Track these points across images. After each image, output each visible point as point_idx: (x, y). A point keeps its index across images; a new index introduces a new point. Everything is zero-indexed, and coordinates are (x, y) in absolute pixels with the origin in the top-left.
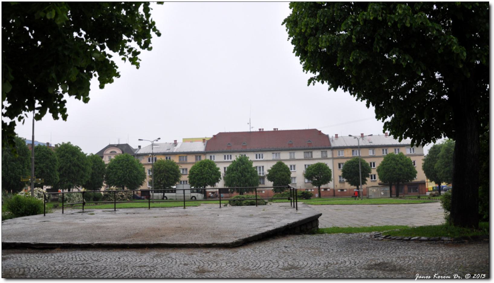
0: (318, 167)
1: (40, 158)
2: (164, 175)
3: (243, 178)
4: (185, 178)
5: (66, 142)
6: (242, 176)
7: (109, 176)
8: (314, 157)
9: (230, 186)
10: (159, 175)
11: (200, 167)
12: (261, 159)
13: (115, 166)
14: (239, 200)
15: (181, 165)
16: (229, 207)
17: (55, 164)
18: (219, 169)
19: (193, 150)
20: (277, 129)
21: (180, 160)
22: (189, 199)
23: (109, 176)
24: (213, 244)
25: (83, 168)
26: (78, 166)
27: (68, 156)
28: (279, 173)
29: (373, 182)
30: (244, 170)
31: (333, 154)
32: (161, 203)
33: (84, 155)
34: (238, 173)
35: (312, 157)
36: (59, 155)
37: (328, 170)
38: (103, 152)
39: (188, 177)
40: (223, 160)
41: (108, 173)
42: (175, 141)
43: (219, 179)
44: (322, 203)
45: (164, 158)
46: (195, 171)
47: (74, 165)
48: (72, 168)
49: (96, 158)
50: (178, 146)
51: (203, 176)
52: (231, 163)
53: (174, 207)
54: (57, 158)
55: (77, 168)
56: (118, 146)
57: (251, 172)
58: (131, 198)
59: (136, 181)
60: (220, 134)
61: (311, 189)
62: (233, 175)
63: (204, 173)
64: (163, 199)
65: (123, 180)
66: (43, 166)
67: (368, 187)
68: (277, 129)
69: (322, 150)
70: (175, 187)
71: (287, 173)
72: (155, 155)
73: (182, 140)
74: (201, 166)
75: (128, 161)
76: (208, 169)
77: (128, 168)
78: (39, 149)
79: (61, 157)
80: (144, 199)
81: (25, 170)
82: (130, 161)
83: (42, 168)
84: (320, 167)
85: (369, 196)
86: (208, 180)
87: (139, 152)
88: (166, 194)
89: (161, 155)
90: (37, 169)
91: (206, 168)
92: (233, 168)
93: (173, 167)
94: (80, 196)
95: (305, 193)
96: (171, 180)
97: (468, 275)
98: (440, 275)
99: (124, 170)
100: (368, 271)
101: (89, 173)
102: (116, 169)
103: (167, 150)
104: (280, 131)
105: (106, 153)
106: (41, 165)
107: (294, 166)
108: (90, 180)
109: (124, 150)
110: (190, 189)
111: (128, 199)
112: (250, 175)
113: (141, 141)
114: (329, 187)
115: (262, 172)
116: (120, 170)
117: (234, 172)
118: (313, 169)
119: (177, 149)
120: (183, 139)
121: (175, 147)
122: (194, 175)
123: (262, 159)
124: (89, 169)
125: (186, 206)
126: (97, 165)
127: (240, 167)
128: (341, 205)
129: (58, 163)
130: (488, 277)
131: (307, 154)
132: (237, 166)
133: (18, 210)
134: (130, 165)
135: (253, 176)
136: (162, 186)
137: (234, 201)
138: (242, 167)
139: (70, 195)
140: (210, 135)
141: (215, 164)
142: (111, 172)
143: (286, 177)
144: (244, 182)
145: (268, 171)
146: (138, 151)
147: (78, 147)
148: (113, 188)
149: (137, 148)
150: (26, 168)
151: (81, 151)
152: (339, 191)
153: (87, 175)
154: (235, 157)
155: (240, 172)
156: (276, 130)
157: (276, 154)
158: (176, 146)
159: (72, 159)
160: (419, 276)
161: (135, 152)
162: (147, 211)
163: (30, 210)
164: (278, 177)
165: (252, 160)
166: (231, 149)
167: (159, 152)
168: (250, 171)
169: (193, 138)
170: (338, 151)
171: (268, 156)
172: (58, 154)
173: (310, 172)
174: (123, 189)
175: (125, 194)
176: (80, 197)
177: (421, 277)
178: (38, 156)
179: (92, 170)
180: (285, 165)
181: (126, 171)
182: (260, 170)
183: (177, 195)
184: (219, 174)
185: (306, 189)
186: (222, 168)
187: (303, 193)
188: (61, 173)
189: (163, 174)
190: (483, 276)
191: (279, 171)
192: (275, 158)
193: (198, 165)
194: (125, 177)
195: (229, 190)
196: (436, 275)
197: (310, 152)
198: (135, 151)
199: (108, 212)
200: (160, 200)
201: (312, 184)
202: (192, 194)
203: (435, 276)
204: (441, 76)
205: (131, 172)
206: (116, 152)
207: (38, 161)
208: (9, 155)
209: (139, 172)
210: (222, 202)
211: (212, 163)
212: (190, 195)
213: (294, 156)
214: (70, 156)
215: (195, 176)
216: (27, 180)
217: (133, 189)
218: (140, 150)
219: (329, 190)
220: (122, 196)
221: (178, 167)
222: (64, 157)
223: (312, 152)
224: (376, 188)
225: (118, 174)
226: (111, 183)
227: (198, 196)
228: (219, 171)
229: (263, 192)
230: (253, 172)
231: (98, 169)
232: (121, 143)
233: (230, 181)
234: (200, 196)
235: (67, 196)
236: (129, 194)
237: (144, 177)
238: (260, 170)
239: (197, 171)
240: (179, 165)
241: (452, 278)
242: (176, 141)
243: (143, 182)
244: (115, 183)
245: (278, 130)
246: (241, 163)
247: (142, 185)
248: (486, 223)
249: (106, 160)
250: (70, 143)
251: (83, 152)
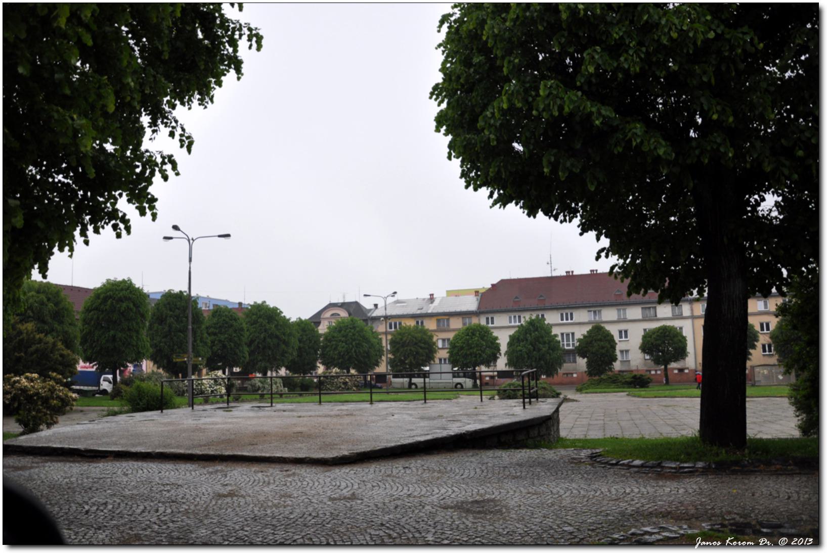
0: (661, 333)
1: (220, 327)
2: (410, 350)
3: (535, 352)
4: (444, 354)
5: (259, 302)
6: (534, 350)
7: (325, 352)
8: (659, 316)
9: (515, 366)
10: (402, 349)
11: (466, 336)
12: (570, 321)
13: (333, 337)
14: (512, 390)
15: (437, 334)
16: (497, 400)
17: (241, 335)
18: (496, 338)
19: (458, 309)
20: (597, 271)
21: (438, 325)
22: (452, 388)
23: (325, 352)
24: (306, 458)
25: (285, 340)
26: (277, 337)
27: (262, 322)
28: (595, 344)
29: (766, 358)
30: (537, 339)
31: (692, 310)
32: (399, 394)
33: (286, 321)
34: (526, 345)
35: (656, 316)
36: (249, 322)
37: (680, 338)
38: (321, 314)
39: (447, 353)
40: (507, 324)
41: (324, 348)
42: (432, 295)
43: (498, 356)
44: (656, 395)
45: (411, 323)
46: (457, 342)
47: (272, 336)
48: (269, 340)
49: (305, 325)
50: (436, 303)
51: (471, 350)
52: (517, 329)
53: (414, 400)
54: (245, 326)
55: (275, 341)
56: (343, 305)
57: (550, 342)
58: (358, 386)
59: (367, 360)
60: (503, 282)
61: (656, 371)
62: (519, 348)
63: (473, 346)
64: (410, 387)
65: (347, 357)
66: (225, 339)
67: (754, 367)
68: (597, 271)
69: (643, 306)
70: (427, 368)
71: (609, 343)
72: (389, 319)
73: (445, 292)
74: (468, 335)
75: (354, 328)
76: (478, 340)
77: (354, 340)
78: (218, 313)
79: (252, 325)
80: (381, 388)
81: (197, 344)
82: (358, 329)
83: (224, 342)
84: (665, 333)
85: (755, 381)
86: (479, 357)
87: (374, 315)
88: (414, 380)
89: (408, 317)
90: (216, 342)
91: (476, 338)
92: (519, 336)
93: (425, 337)
94: (280, 383)
95: (638, 376)
96: (421, 358)
98: (737, 540)
99: (348, 342)
100: (285, 502)
101: (293, 348)
102: (337, 341)
103: (419, 309)
104: (600, 274)
105: (324, 317)
106: (222, 337)
107: (626, 332)
108: (296, 359)
109: (351, 312)
110: (451, 371)
111: (354, 388)
112: (547, 348)
113: (368, 297)
114: (687, 366)
115: (571, 343)
116: (343, 342)
117: (521, 343)
118: (654, 336)
119: (433, 309)
120: (447, 291)
121: (431, 305)
122: (457, 349)
123: (572, 321)
124: (295, 342)
125: (428, 399)
126: (306, 335)
127: (531, 334)
128: (689, 397)
129: (246, 334)
130: (817, 543)
131: (647, 311)
132: (526, 333)
133: (138, 404)
134: (357, 334)
135: (552, 350)
136: (408, 366)
137: (505, 391)
138: (533, 334)
139: (265, 381)
140: (486, 283)
141: (490, 331)
142: (329, 346)
143: (607, 351)
144: (538, 360)
145: (579, 340)
146: (373, 313)
147: (277, 308)
148: (335, 370)
149: (372, 307)
150: (198, 342)
151: (283, 315)
152: (676, 371)
153: (290, 351)
154: (526, 317)
155: (531, 344)
156: (595, 272)
157: (595, 312)
158: (432, 303)
159: (268, 326)
160: (702, 541)
161: (369, 315)
162: (367, 405)
163: (154, 403)
164: (594, 350)
165: (551, 322)
166: (519, 306)
167: (405, 313)
168: (547, 342)
169: (458, 290)
170: (701, 305)
171: (582, 316)
172: (247, 320)
173: (649, 341)
174: (348, 372)
175: (350, 381)
176: (278, 385)
178: (217, 324)
179: (298, 343)
180: (606, 330)
181: (352, 344)
182: (568, 340)
183: (431, 381)
184: (497, 348)
185: (647, 371)
186: (503, 340)
187: (635, 377)
188: (252, 348)
189: (409, 348)
190: (808, 542)
191: (596, 341)
192: (593, 319)
193: (463, 333)
194: (350, 354)
195: (514, 373)
196: (729, 539)
197: (653, 307)
198: (368, 313)
199: (256, 409)
200: (404, 389)
201: (653, 362)
202: (454, 379)
203: (728, 541)
205: (358, 345)
206: (339, 315)
207: (217, 331)
208: (175, 323)
209: (372, 345)
210: (484, 393)
211: (485, 330)
212: (451, 381)
213: (625, 314)
214: (265, 322)
215: (458, 350)
216: (183, 360)
217: (364, 373)
218: (377, 310)
219: (686, 371)
220: (345, 383)
221: (431, 337)
222: (256, 324)
223: (655, 308)
224: (769, 368)
225: (340, 349)
226: (328, 363)
227: (465, 382)
228: (498, 341)
229: (575, 375)
230: (552, 343)
231: (308, 341)
232: (348, 300)
233: (515, 358)
234: (468, 383)
235: (259, 384)
236: (356, 380)
237: (380, 352)
238: (568, 340)
239: (462, 343)
240: (433, 333)
241: (757, 545)
242: (433, 295)
243: (379, 360)
244: (335, 362)
245: (598, 272)
246: (532, 329)
247: (378, 366)
249: (323, 329)
250: (265, 302)
251: (284, 316)
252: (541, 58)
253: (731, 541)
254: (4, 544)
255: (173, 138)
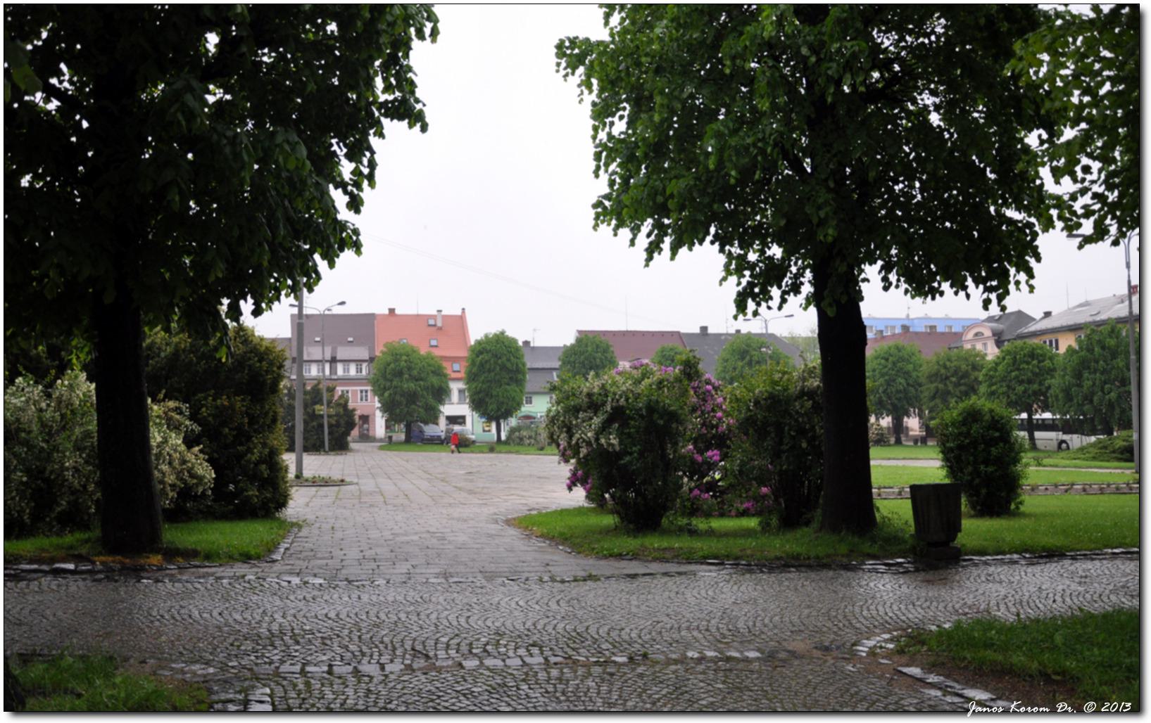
97: (1090, 705)
130: (1137, 709)
177: (980, 709)
190: (1125, 707)
204: (1018, 131)
227: (1071, 440)
241: (1053, 712)
248: (8, 572)
252: (337, 83)
253: (1018, 707)
254: (5, 710)
255: (384, 137)
